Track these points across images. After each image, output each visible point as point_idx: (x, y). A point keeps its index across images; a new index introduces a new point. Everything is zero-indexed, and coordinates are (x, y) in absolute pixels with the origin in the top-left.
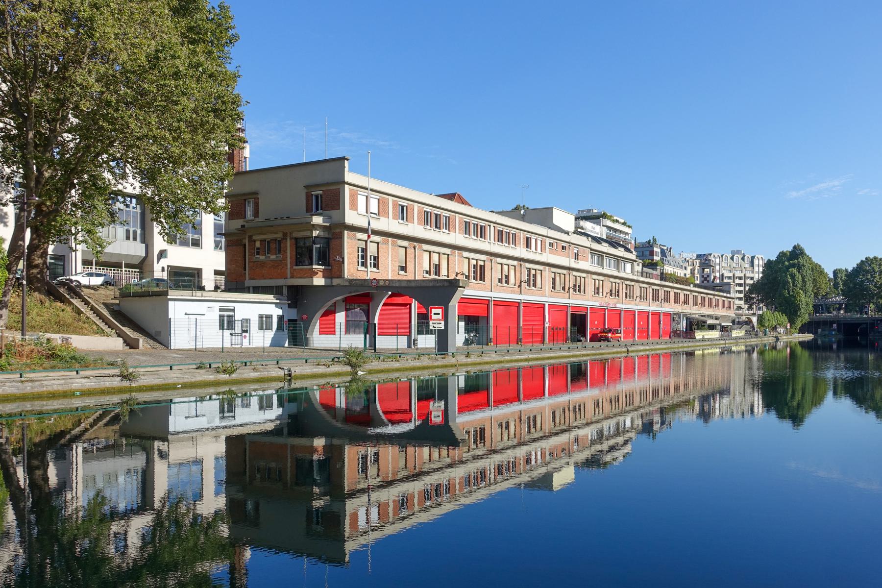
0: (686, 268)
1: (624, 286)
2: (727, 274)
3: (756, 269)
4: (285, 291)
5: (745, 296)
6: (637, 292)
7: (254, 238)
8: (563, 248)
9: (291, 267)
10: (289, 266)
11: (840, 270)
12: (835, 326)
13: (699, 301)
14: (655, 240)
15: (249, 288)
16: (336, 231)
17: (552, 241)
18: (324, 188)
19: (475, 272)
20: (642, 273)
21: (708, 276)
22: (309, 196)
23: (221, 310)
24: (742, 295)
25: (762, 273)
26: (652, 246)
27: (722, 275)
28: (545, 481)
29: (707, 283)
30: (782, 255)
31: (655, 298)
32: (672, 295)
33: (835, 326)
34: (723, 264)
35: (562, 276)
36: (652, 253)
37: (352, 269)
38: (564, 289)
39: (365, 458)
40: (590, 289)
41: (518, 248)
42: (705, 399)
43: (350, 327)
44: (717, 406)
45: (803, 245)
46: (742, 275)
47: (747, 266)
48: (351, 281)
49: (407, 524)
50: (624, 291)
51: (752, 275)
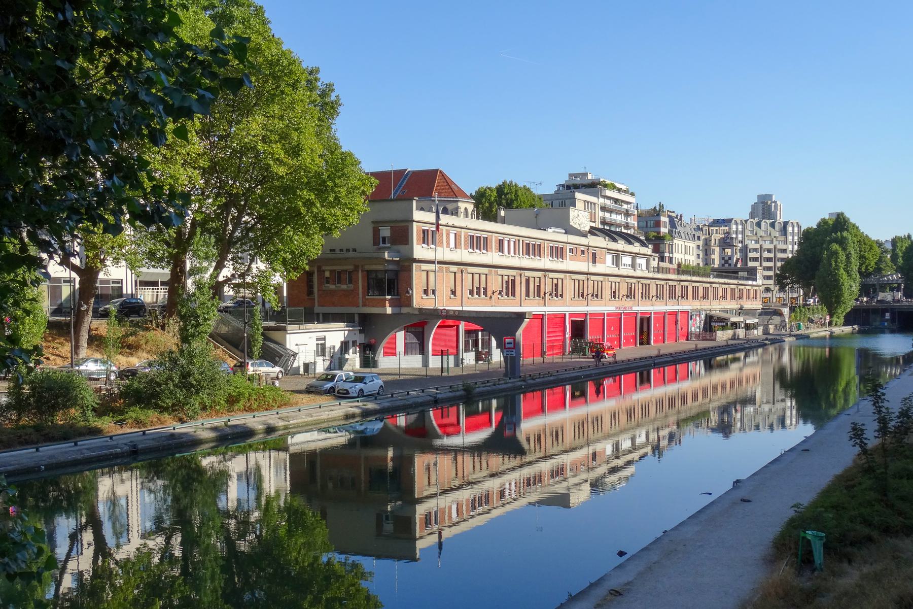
0: (699, 238)
1: (640, 286)
2: (752, 245)
3: (790, 238)
4: (357, 318)
5: (776, 275)
6: (653, 291)
7: (323, 268)
8: (583, 252)
9: (364, 297)
10: (361, 296)
11: (900, 239)
12: (888, 316)
13: (720, 294)
14: (661, 206)
15: (318, 314)
16: (407, 263)
17: (571, 247)
18: (392, 225)
19: (507, 288)
20: (658, 268)
21: (730, 258)
22: (376, 232)
23: (318, 339)
24: (771, 273)
25: (800, 244)
26: (658, 215)
27: (746, 247)
28: (562, 500)
29: (727, 271)
30: (823, 223)
31: (672, 295)
32: (690, 289)
33: (888, 316)
34: (747, 233)
35: (581, 282)
36: (658, 224)
37: (419, 300)
38: (582, 296)
39: (428, 465)
40: (607, 293)
41: (542, 259)
42: (725, 409)
43: (408, 350)
44: (739, 416)
45: (847, 215)
46: (772, 247)
47: (777, 234)
48: (420, 309)
49: (508, 508)
50: (640, 291)
51: (784, 247)
